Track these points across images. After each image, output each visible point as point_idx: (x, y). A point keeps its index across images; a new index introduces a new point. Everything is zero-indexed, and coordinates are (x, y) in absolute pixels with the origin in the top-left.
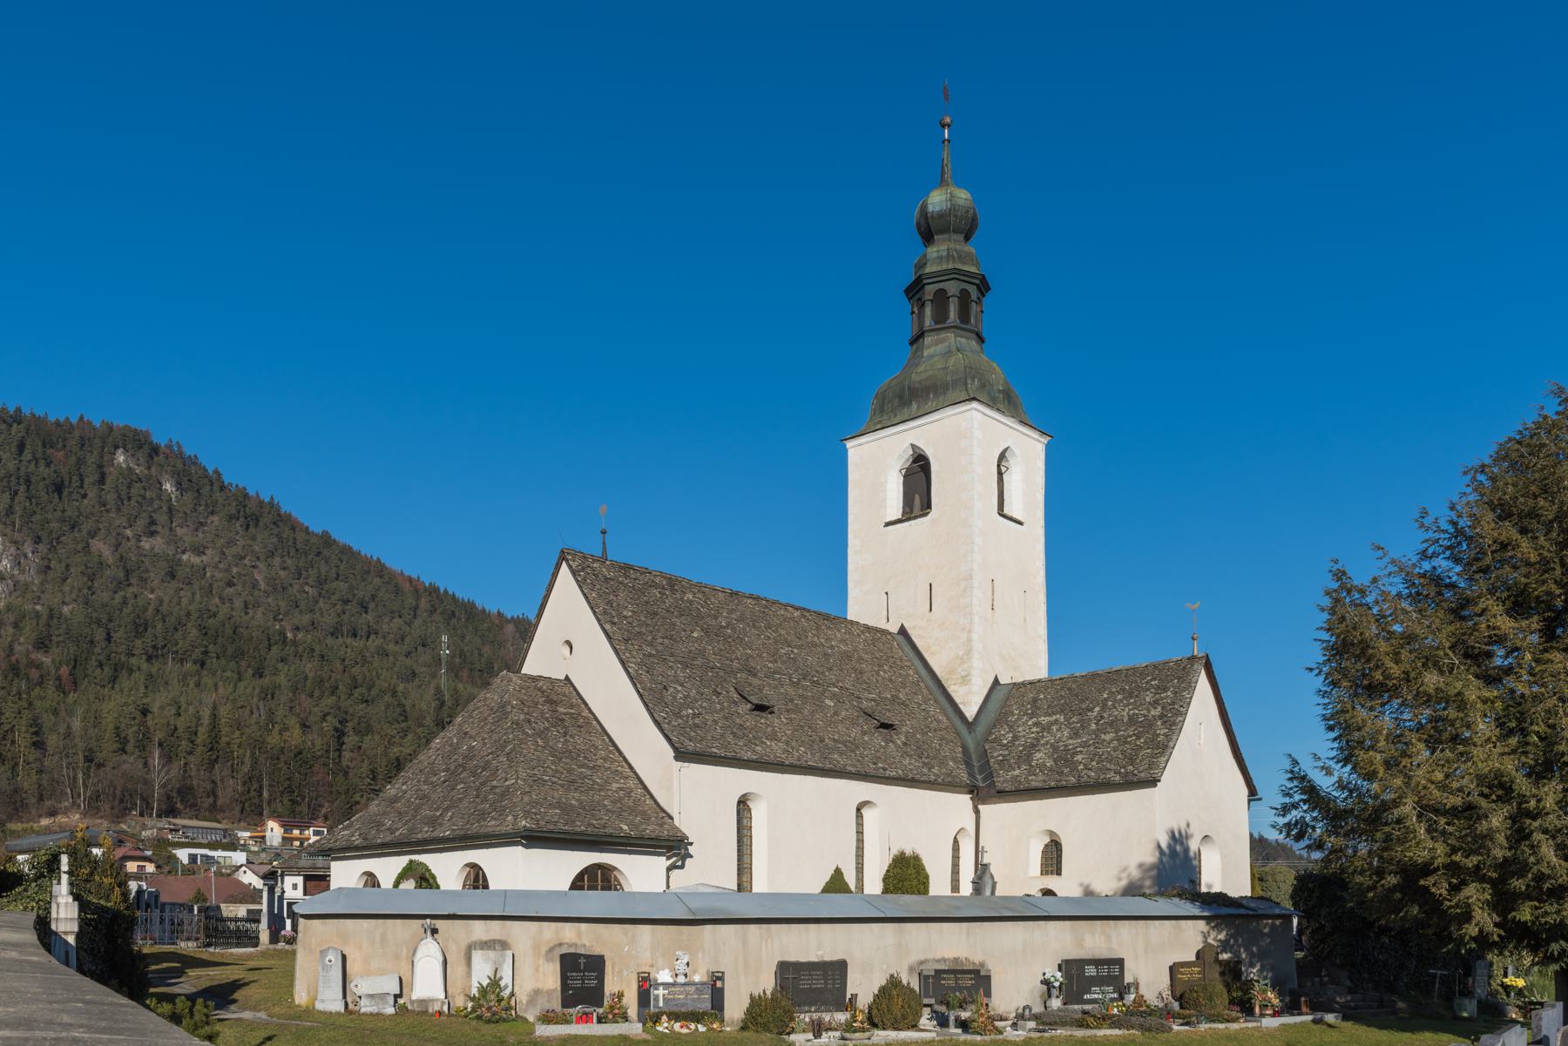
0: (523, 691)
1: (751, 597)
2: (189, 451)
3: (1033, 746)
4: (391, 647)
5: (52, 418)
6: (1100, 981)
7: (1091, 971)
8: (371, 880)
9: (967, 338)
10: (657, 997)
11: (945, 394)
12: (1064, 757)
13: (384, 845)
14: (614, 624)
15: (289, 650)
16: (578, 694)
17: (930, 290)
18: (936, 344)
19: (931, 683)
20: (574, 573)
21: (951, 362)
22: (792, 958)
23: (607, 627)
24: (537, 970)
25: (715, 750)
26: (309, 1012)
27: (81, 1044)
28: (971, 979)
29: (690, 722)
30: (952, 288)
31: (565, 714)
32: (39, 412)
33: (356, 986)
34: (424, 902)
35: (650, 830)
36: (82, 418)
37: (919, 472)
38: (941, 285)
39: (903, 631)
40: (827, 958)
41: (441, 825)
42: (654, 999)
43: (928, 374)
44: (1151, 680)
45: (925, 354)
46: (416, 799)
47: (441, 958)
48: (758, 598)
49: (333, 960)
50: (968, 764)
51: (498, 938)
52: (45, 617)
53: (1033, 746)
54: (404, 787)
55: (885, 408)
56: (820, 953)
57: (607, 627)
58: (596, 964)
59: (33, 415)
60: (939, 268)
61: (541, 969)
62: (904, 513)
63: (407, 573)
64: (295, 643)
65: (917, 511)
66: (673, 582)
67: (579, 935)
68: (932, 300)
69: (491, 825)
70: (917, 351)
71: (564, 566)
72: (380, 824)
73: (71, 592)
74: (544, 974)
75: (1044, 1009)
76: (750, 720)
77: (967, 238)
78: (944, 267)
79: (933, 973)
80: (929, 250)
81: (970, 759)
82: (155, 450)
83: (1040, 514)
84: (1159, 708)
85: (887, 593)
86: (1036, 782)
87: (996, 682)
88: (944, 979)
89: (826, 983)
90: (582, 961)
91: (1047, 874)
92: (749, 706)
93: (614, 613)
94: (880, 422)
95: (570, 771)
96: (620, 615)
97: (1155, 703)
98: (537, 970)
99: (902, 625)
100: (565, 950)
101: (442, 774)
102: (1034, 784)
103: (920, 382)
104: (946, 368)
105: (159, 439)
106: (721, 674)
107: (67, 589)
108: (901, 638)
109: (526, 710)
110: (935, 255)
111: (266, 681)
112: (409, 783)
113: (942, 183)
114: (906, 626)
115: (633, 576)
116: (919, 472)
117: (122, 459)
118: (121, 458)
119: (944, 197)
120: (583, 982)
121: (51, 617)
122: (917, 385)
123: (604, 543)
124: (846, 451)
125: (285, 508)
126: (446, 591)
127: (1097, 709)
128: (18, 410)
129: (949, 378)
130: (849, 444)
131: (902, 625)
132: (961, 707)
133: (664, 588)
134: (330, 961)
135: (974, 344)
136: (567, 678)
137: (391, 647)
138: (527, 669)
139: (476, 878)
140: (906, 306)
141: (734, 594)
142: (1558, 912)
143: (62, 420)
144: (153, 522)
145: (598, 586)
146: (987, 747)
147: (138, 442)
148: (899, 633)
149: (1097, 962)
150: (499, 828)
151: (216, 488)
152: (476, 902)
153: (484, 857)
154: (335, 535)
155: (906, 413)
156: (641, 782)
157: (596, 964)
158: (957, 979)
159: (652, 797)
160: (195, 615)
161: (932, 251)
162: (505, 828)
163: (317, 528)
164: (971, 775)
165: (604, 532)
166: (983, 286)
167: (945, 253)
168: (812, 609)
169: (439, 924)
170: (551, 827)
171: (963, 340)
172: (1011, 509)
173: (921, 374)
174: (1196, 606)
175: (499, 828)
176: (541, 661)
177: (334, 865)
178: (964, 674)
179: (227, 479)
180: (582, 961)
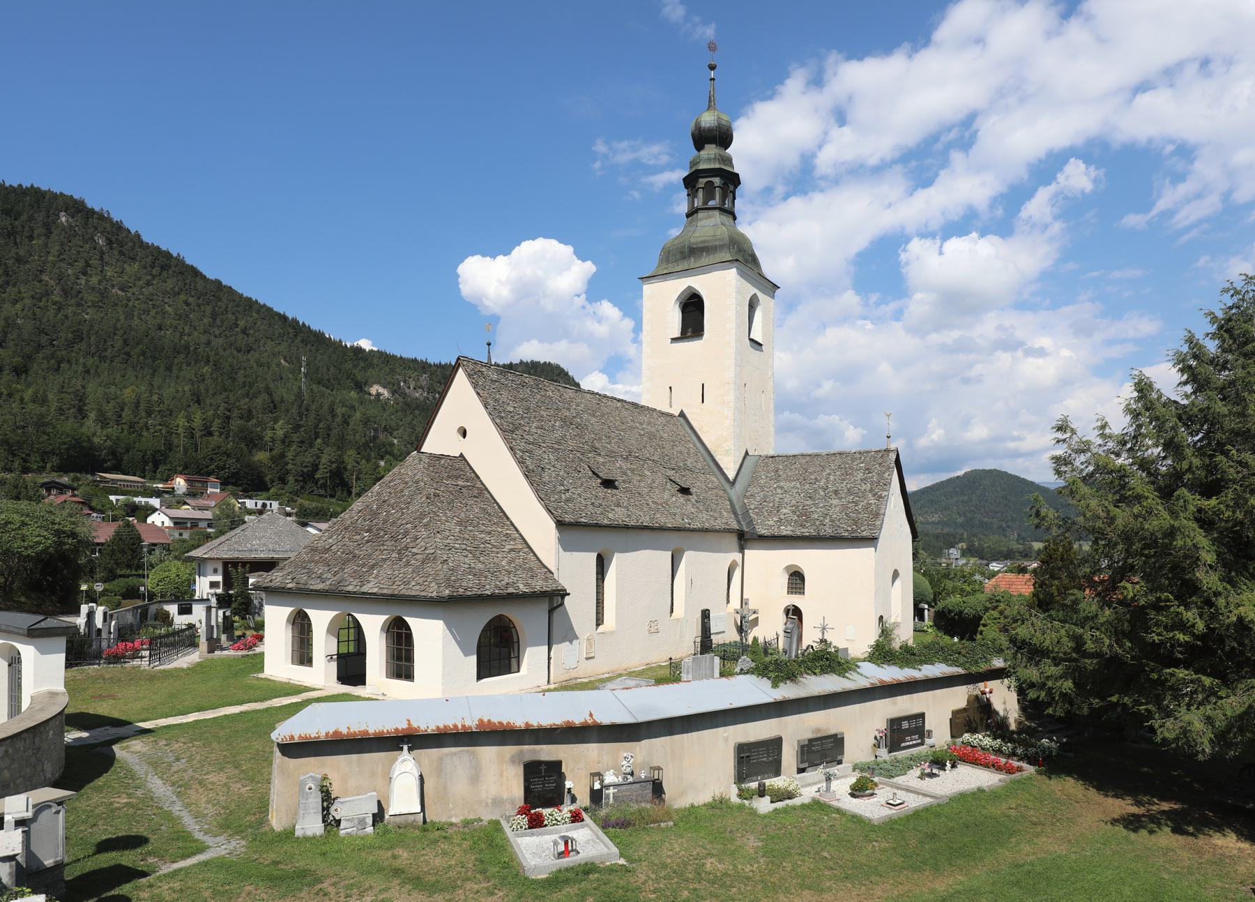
0: (431, 469)
2: (116, 217)
7: (905, 725)
10: (608, 796)
14: (502, 418)
16: (471, 468)
18: (706, 218)
19: (704, 453)
20: (469, 376)
23: (498, 421)
24: (501, 775)
25: (582, 520)
26: (288, 835)
27: (3, 278)
28: (831, 742)
33: (336, 810)
38: (710, 179)
39: (682, 414)
42: (605, 798)
44: (860, 463)
45: (699, 224)
46: (343, 553)
49: (313, 787)
50: (735, 513)
54: (330, 541)
55: (670, 259)
57: (498, 421)
58: (555, 768)
61: (505, 774)
68: (703, 188)
70: (691, 222)
74: (508, 779)
75: (874, 758)
76: (602, 492)
79: (807, 743)
80: (702, 153)
85: (670, 388)
87: (747, 453)
88: (814, 746)
90: (543, 767)
91: (792, 593)
92: (599, 481)
94: (666, 268)
95: (474, 538)
98: (501, 775)
101: (365, 534)
102: (784, 533)
103: (696, 244)
106: (578, 454)
108: (681, 419)
109: (435, 485)
110: (706, 156)
112: (335, 537)
114: (685, 411)
115: (510, 378)
116: (692, 307)
117: (64, 219)
119: (712, 118)
120: (544, 786)
123: (489, 352)
125: (189, 261)
126: (303, 323)
132: (725, 471)
134: (310, 789)
136: (461, 455)
144: (88, 265)
145: (487, 387)
146: (746, 501)
148: (679, 416)
156: (526, 542)
157: (555, 768)
159: (535, 555)
160: (120, 332)
162: (430, 595)
163: (211, 275)
164: (739, 522)
165: (489, 344)
167: (713, 156)
168: (628, 400)
178: (727, 448)
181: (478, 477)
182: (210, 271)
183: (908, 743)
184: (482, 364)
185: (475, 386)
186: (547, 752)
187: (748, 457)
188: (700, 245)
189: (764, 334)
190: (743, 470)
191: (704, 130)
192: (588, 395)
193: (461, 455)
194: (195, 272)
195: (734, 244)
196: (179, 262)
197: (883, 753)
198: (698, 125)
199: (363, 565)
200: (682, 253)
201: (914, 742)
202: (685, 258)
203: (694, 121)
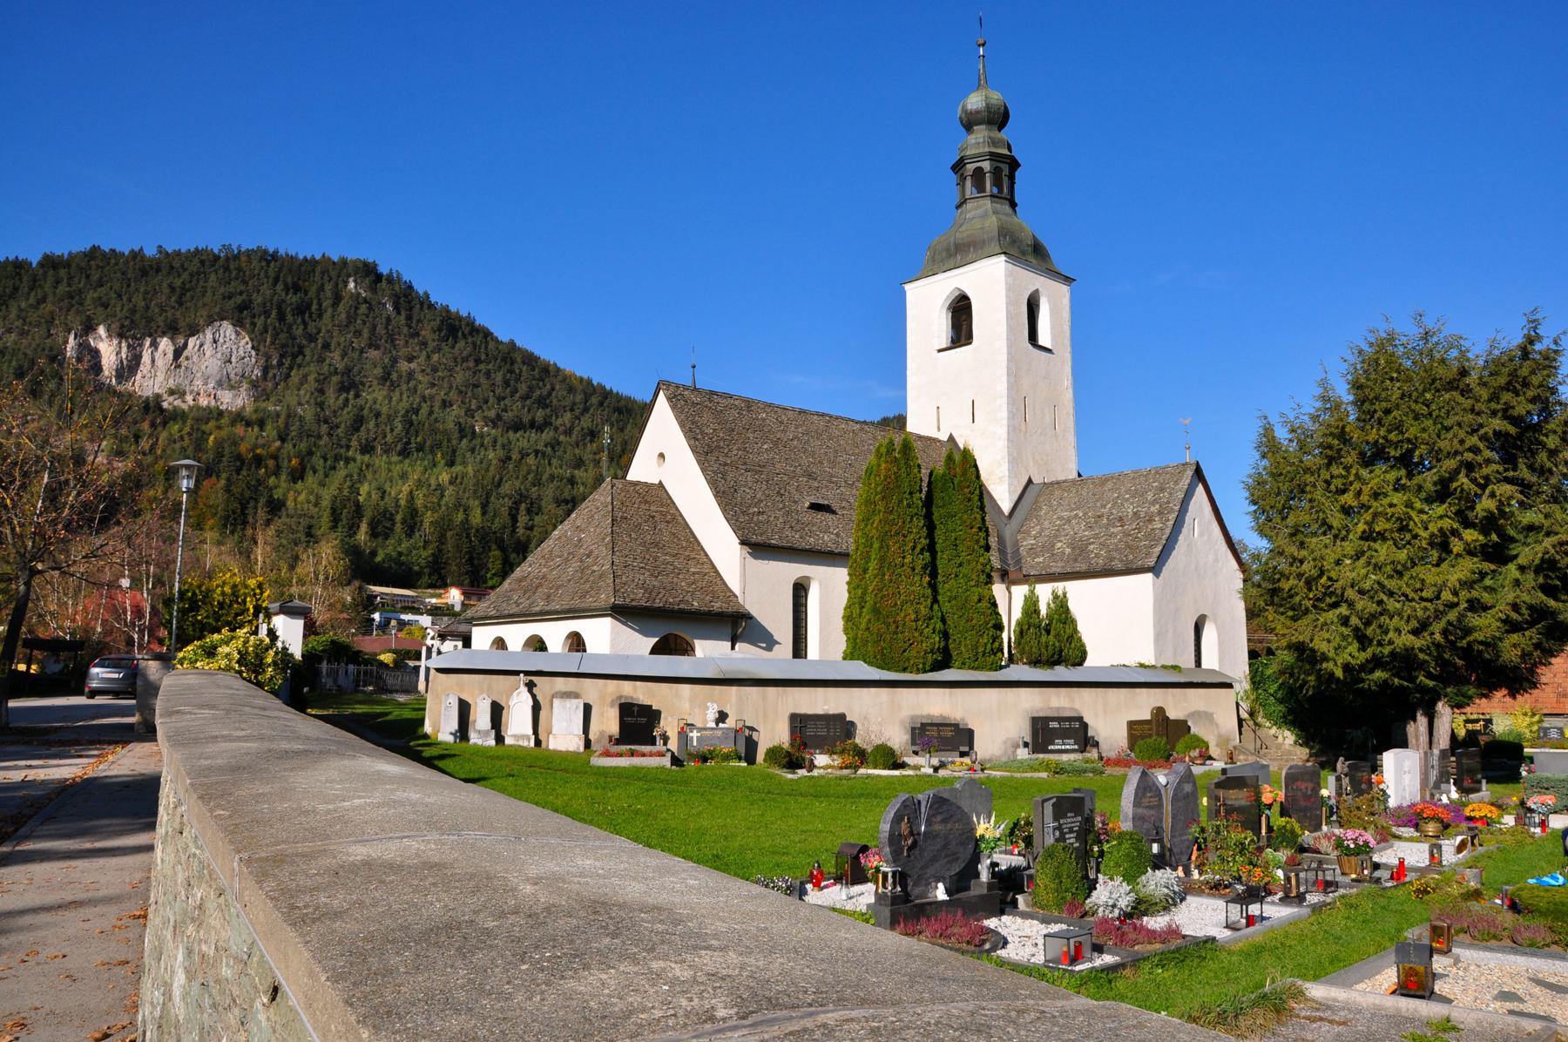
1: (818, 414)
3: (1056, 536)
4: (562, 438)
5: (301, 257)
6: (1064, 734)
7: (1054, 725)
8: (500, 643)
9: (1002, 204)
11: (982, 248)
12: (1080, 548)
13: (542, 613)
15: (477, 441)
17: (971, 167)
20: (669, 399)
21: (987, 223)
22: (803, 711)
29: (755, 518)
30: (986, 165)
31: (656, 512)
32: (292, 252)
34: (536, 662)
35: (717, 606)
36: (324, 255)
37: (961, 310)
40: (831, 712)
41: (553, 600)
43: (970, 232)
47: (531, 703)
48: (823, 415)
51: (574, 690)
52: (283, 417)
53: (1056, 536)
56: (826, 707)
59: (287, 255)
60: (977, 151)
62: (953, 341)
63: (578, 374)
64: (482, 436)
65: (963, 339)
66: (749, 404)
67: (635, 689)
69: (589, 602)
71: (661, 394)
72: (510, 598)
73: (305, 395)
77: (1000, 129)
78: (981, 151)
81: (1005, 547)
82: (379, 277)
83: (1067, 342)
84: (1157, 506)
86: (1057, 568)
87: (1030, 481)
88: (928, 730)
89: (828, 731)
90: (636, 709)
93: (698, 431)
96: (702, 432)
97: (1153, 503)
99: (951, 435)
100: (623, 701)
103: (962, 239)
104: (983, 228)
105: (384, 269)
106: (786, 478)
107: (302, 392)
110: (973, 141)
111: (458, 469)
113: (979, 87)
116: (961, 310)
118: (352, 285)
121: (289, 416)
122: (960, 242)
124: (904, 293)
127: (1109, 506)
128: (276, 252)
129: (985, 236)
130: (907, 287)
131: (951, 435)
133: (741, 409)
135: (1007, 208)
136: (660, 482)
137: (562, 438)
138: (630, 477)
139: (576, 642)
140: (954, 178)
141: (802, 412)
142: (1241, 682)
143: (309, 257)
147: (368, 272)
149: (1060, 719)
150: (595, 604)
151: (425, 306)
152: (572, 663)
153: (580, 626)
154: (519, 343)
155: (951, 262)
158: (939, 731)
161: (972, 139)
165: (694, 367)
166: (1014, 164)
167: (982, 140)
169: (535, 679)
170: (634, 603)
171: (998, 206)
172: (1044, 338)
173: (964, 233)
174: (1187, 422)
175: (595, 604)
176: (642, 469)
177: (475, 630)
179: (433, 300)
180: (636, 709)
181: (674, 504)
182: (503, 333)
183: (1059, 747)
184: (686, 388)
185: (673, 407)
186: (641, 694)
187: (1031, 486)
188: (966, 241)
189: (1054, 338)
190: (1023, 502)
191: (971, 113)
192: (815, 417)
193: (660, 482)
194: (487, 334)
195: (1005, 237)
196: (470, 323)
197: (1023, 754)
198: (965, 110)
199: (551, 588)
200: (948, 250)
201: (1068, 747)
202: (951, 256)
203: (960, 108)
